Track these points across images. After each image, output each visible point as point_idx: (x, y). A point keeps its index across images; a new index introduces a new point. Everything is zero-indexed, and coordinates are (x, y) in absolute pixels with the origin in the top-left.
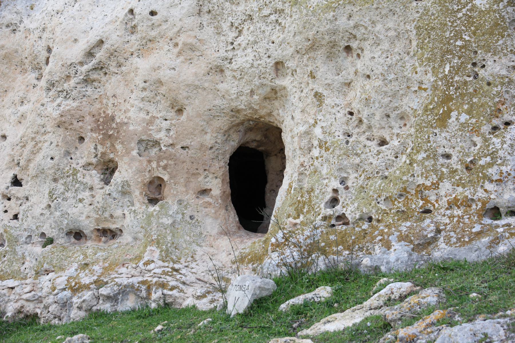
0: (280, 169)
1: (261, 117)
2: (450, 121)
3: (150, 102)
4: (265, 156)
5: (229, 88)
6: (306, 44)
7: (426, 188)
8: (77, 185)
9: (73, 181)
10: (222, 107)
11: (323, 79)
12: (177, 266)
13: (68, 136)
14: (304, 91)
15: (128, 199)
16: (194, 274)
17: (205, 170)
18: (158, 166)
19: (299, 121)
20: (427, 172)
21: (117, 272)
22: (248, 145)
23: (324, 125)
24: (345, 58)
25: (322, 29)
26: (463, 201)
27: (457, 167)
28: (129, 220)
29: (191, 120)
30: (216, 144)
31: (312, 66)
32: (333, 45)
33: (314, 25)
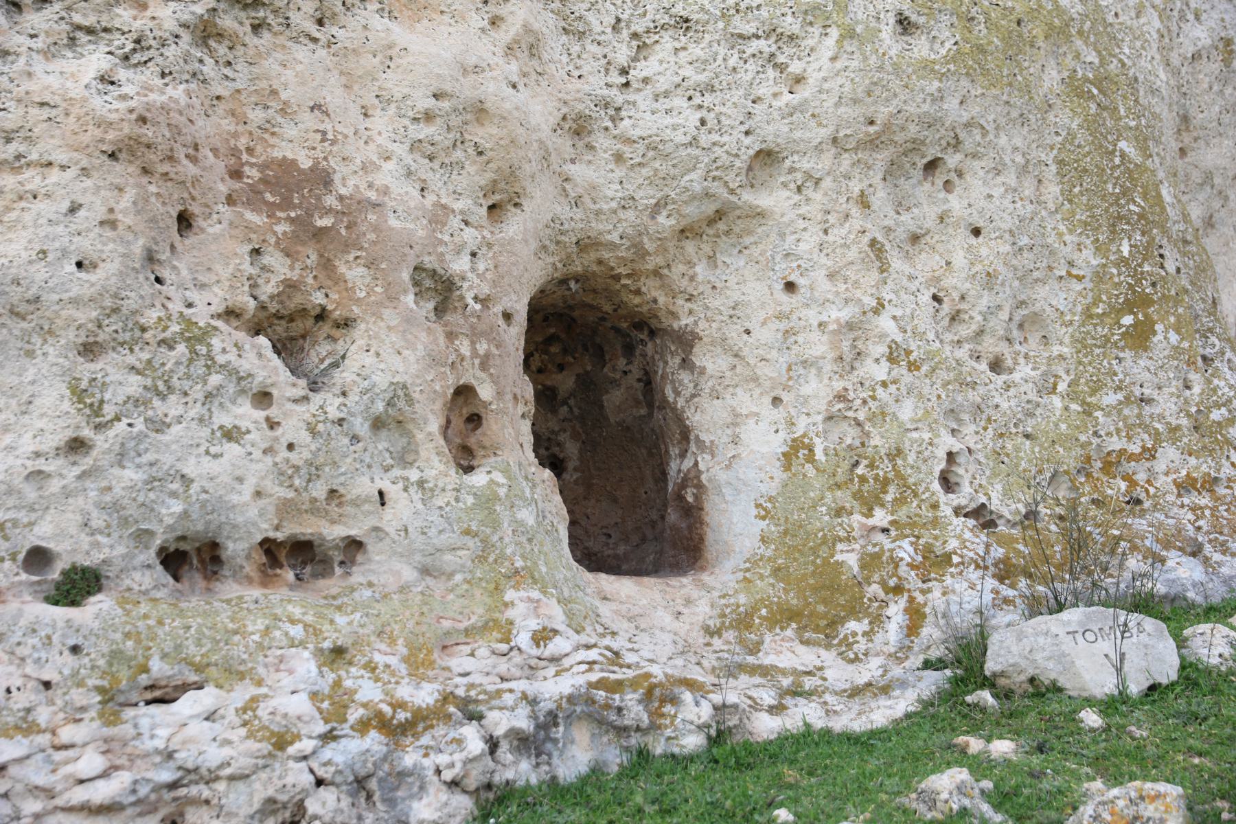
2: (1155, 339)
5: (601, 181)
6: (864, 129)
7: (1132, 457)
8: (215, 379)
9: (191, 360)
10: (566, 226)
13: (153, 199)
15: (386, 445)
19: (830, 296)
20: (1129, 427)
23: (899, 313)
24: (920, 183)
25: (911, 109)
26: (1205, 482)
27: (1179, 422)
28: (403, 508)
31: (861, 180)
32: (916, 146)
33: (895, 95)
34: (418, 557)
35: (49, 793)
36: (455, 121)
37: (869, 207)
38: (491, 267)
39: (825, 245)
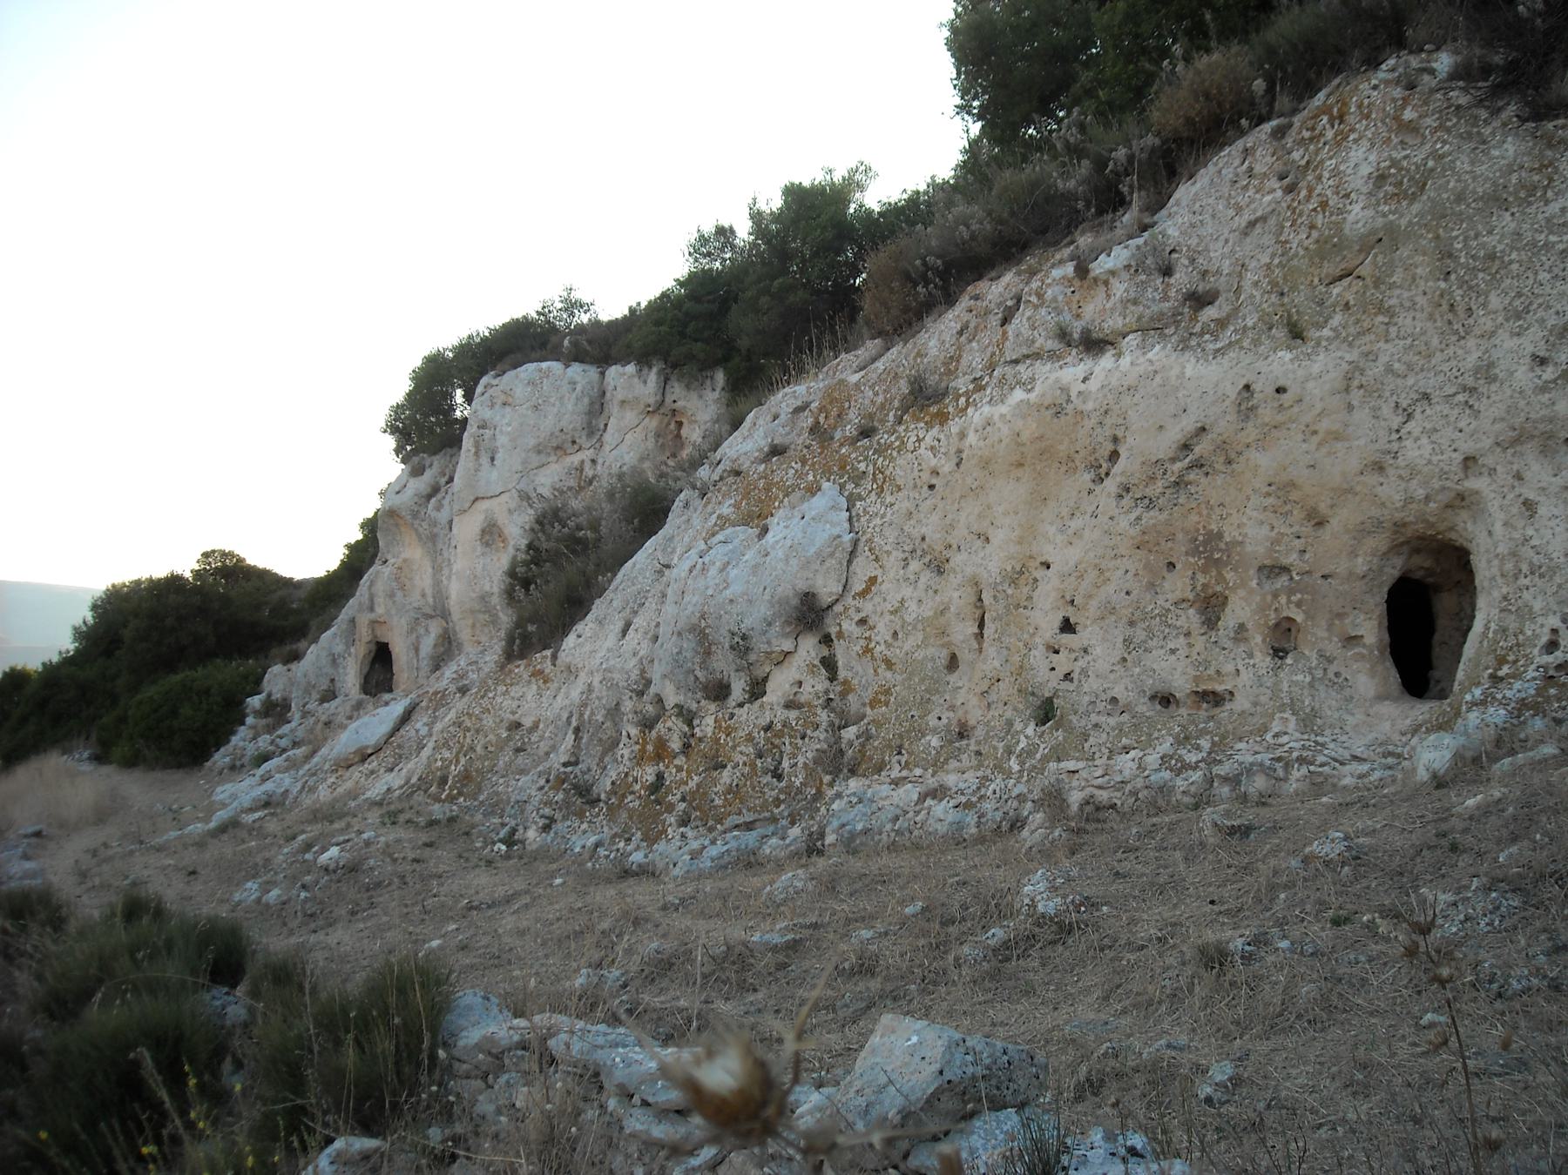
18: (1289, 601)
28: (1246, 677)
35: (1087, 780)
36: (1280, 493)
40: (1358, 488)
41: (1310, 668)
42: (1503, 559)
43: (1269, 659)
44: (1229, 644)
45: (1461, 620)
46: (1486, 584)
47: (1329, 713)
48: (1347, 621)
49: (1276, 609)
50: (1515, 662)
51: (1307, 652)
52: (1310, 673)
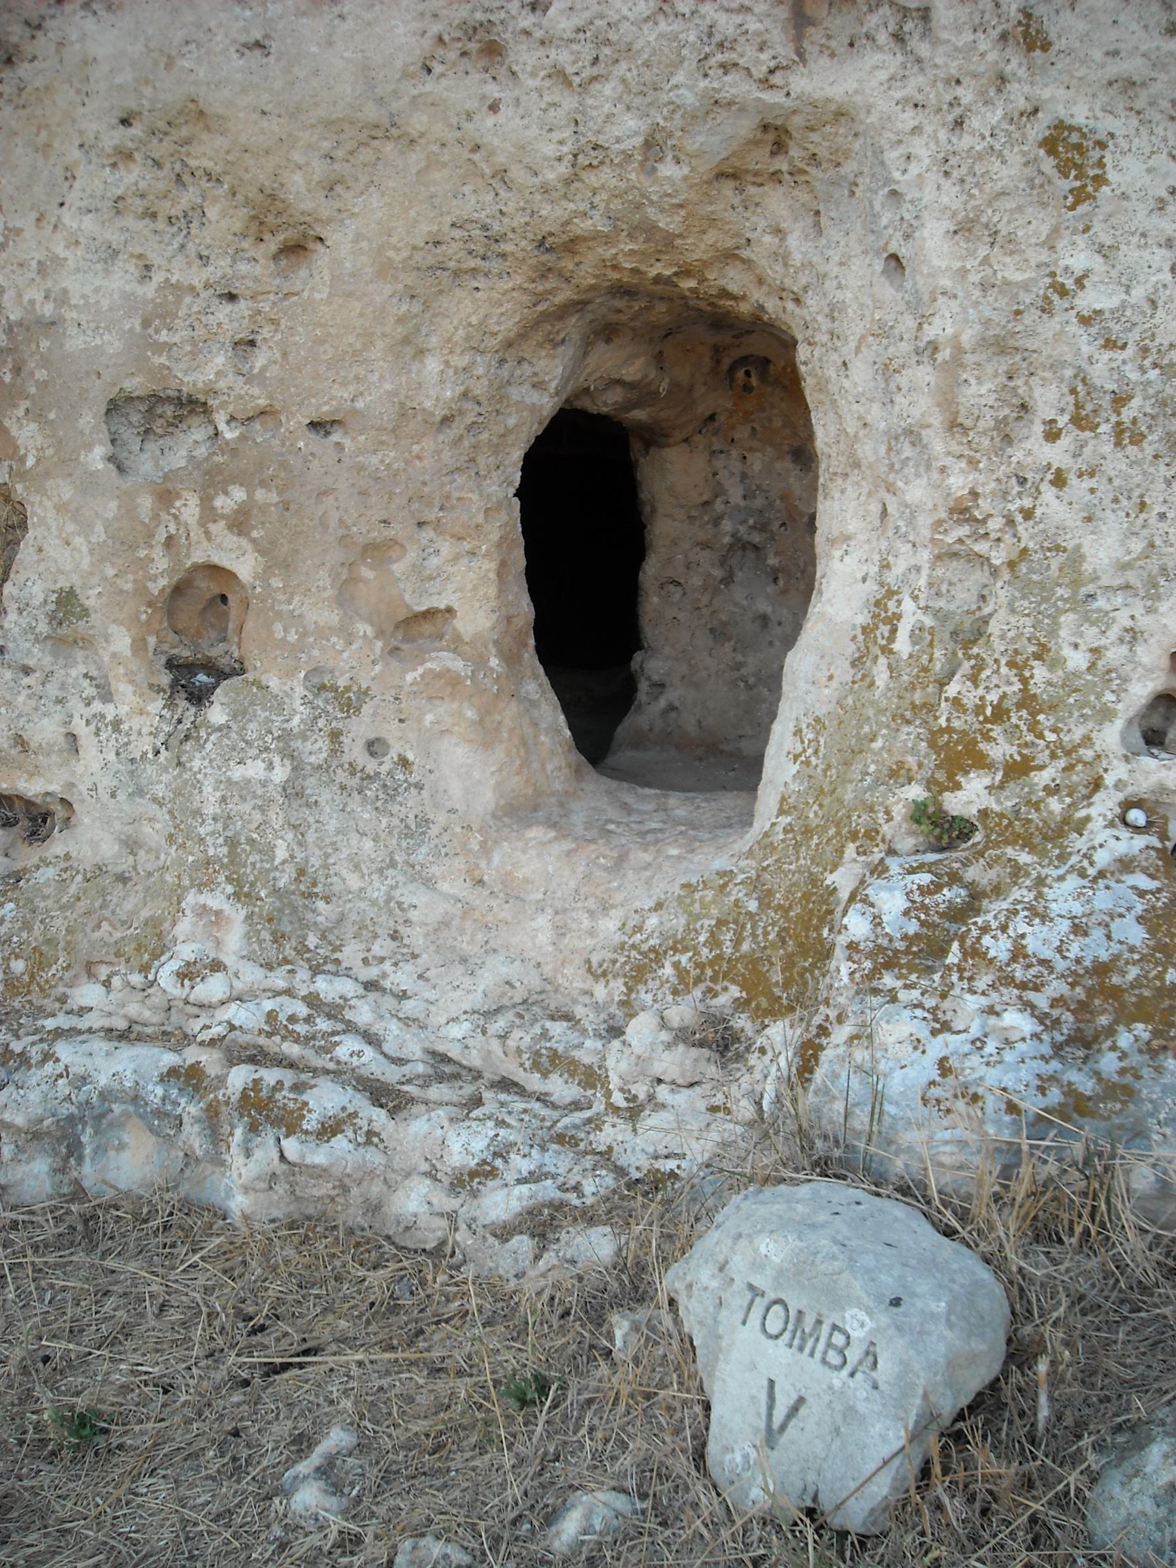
0: (705, 498)
1: (686, 272)
3: (154, 216)
4: (636, 446)
11: (1098, 55)
12: (327, 988)
14: (974, 123)
16: (414, 1029)
17: (420, 524)
18: (209, 514)
21: (63, 999)
22: (586, 404)
29: (350, 295)
30: (469, 405)
34: (117, 825)
36: (161, 149)
37: (1046, 46)
38: (278, 356)
39: (953, 161)
40: (418, 122)
41: (286, 736)
42: (957, 361)
43: (156, 705)
44: (38, 656)
45: (717, 521)
46: (870, 450)
47: (354, 882)
48: (398, 568)
49: (170, 541)
50: (1018, 769)
51: (274, 683)
52: (289, 754)
